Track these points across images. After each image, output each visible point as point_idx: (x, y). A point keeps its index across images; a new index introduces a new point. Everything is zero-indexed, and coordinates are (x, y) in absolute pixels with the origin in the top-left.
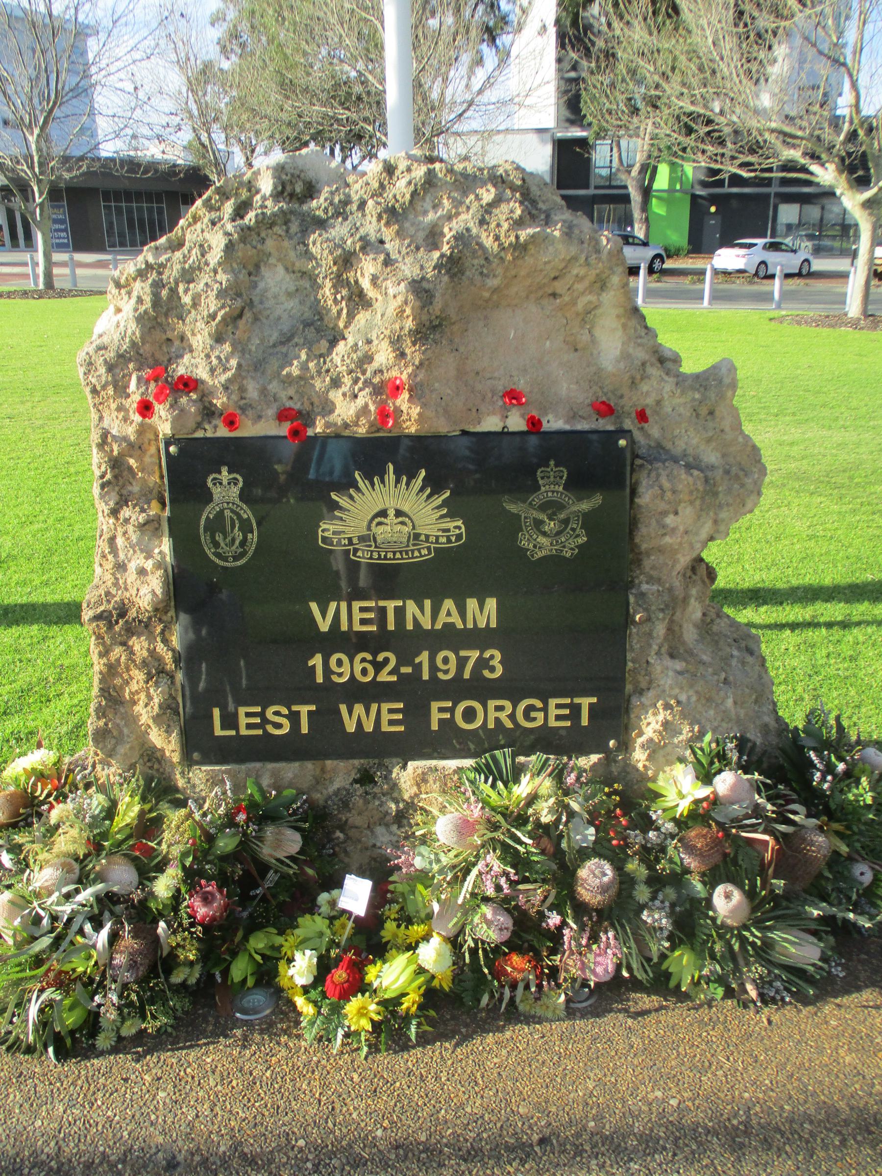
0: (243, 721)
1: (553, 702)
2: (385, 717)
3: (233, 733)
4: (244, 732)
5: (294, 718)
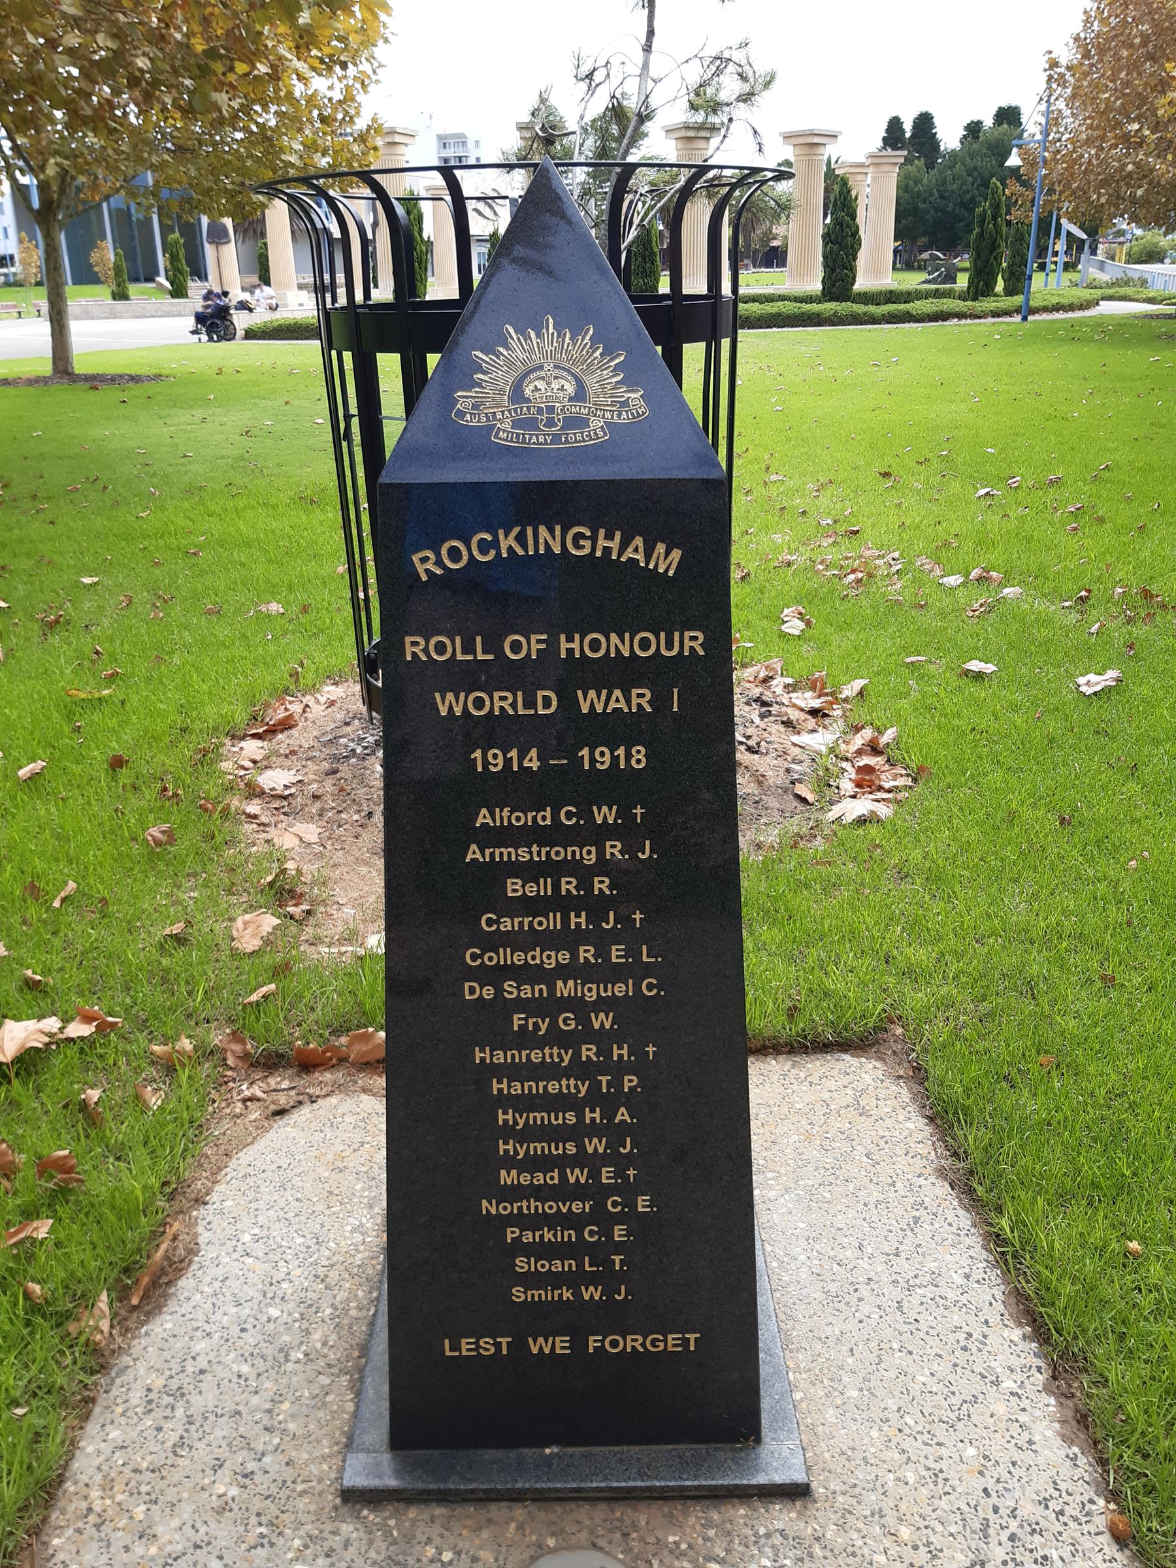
0: (464, 1347)
1: (670, 1337)
2: (558, 1345)
3: (457, 1354)
4: (464, 1353)
5: (498, 1346)
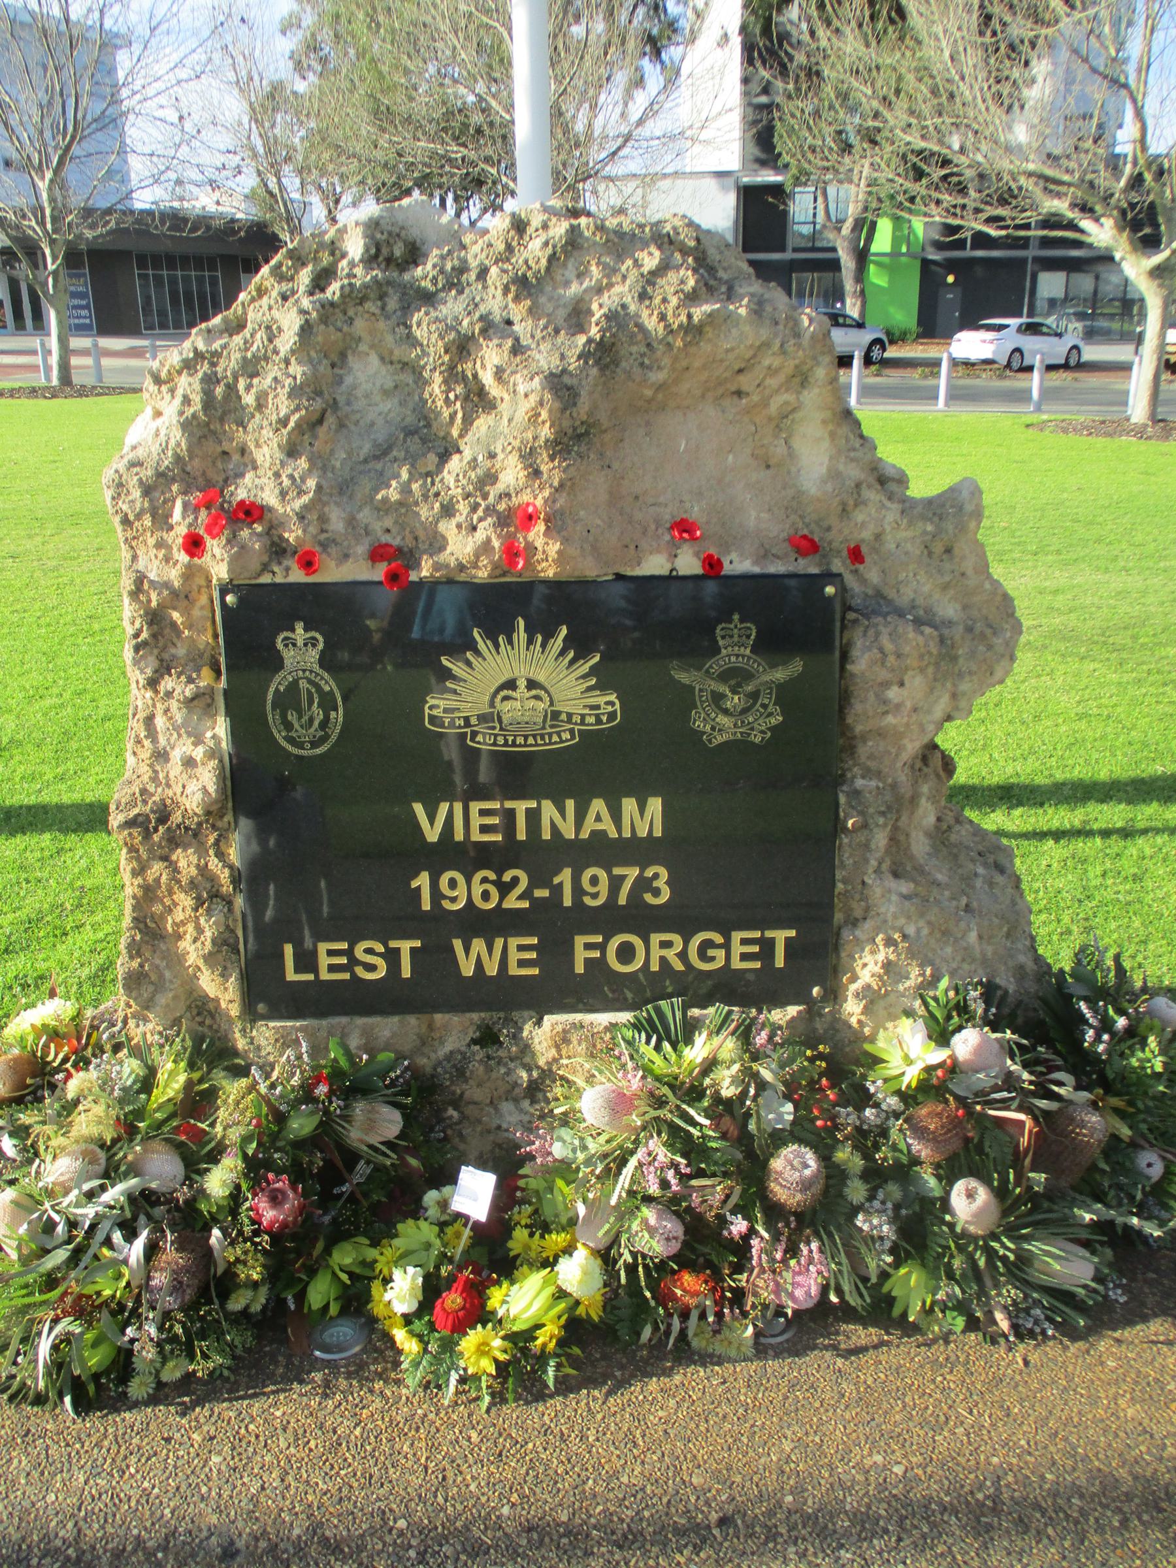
0: (324, 961)
1: (737, 936)
2: (514, 956)
3: (311, 977)
4: (325, 976)
5: (392, 957)
